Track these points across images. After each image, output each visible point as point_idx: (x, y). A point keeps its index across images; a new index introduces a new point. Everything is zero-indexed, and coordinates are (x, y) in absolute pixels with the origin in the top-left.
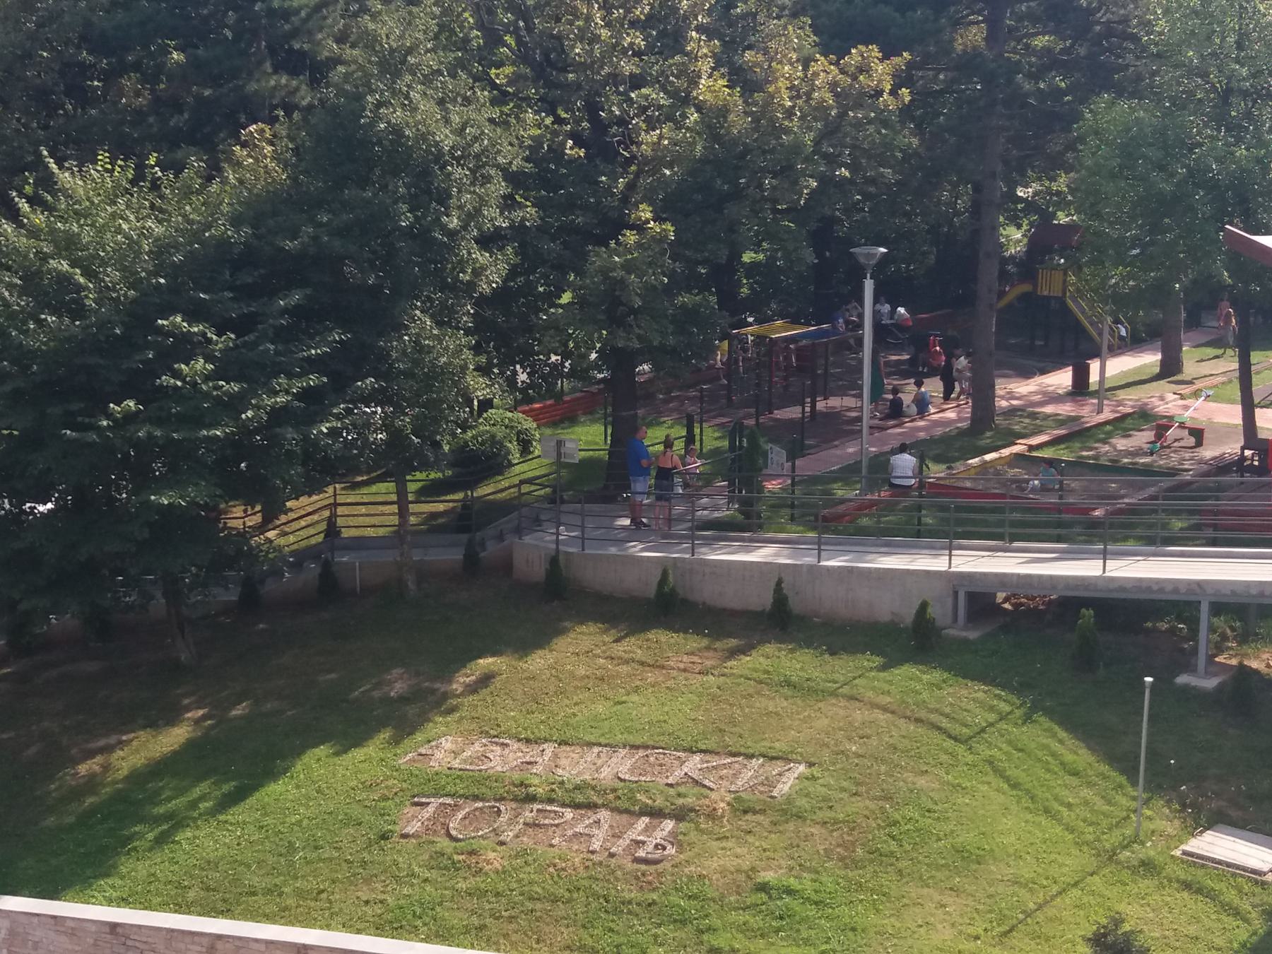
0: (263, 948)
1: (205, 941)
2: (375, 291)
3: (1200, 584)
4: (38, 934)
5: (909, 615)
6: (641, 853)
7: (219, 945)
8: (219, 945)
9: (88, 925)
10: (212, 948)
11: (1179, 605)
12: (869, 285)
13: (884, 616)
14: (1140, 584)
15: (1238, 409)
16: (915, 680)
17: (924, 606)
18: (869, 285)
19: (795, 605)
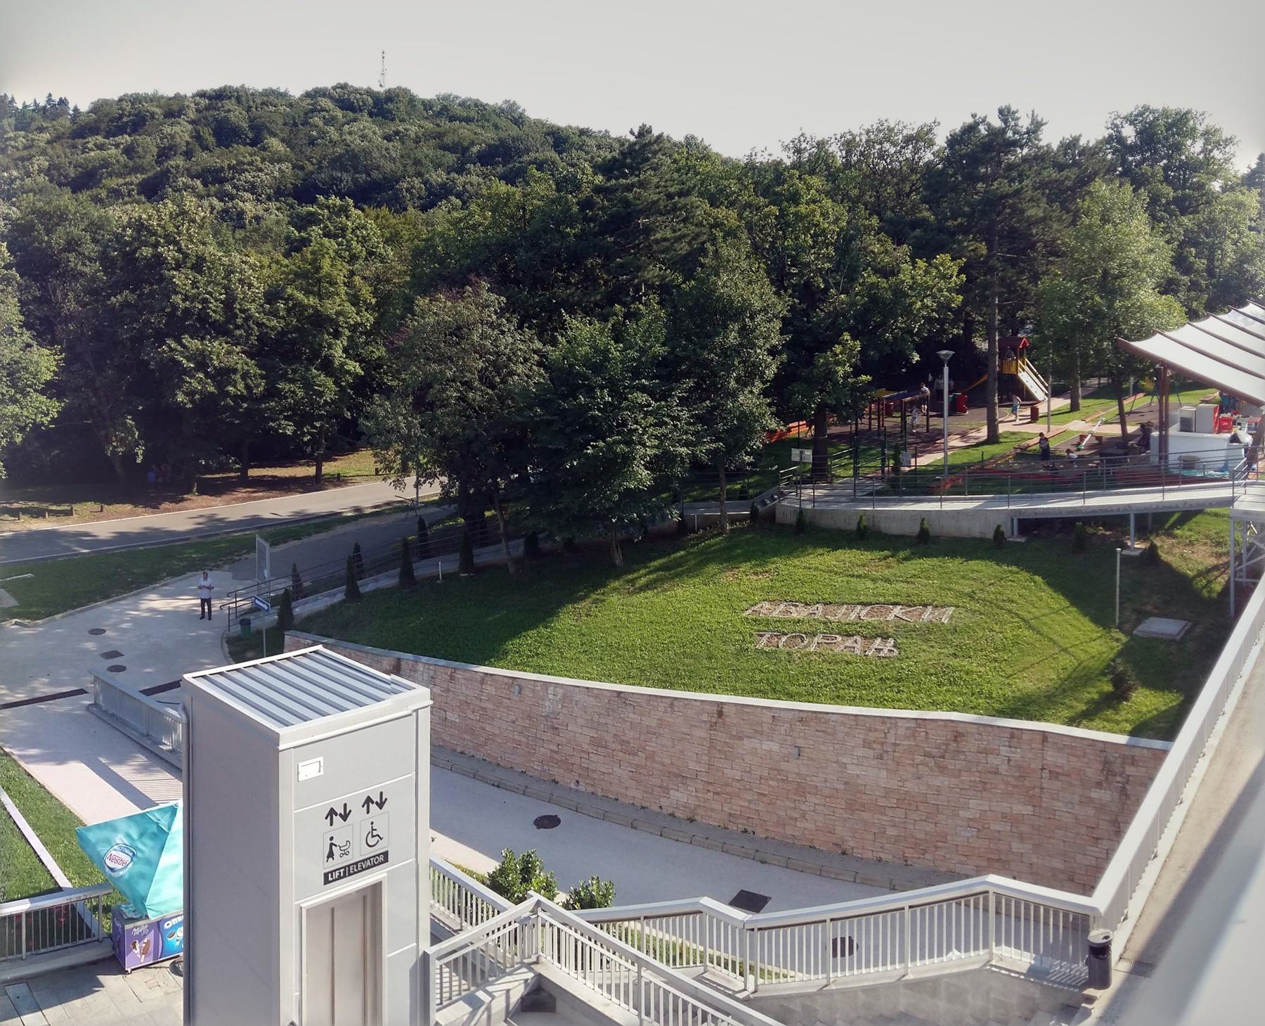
0: (913, 725)
1: (668, 701)
2: (614, 565)
3: (1129, 505)
4: (577, 697)
5: (990, 535)
6: (882, 654)
7: (676, 703)
8: (676, 703)
9: (782, 713)
10: (672, 705)
11: (1115, 520)
12: (946, 369)
13: (977, 535)
14: (1102, 508)
15: (1119, 426)
16: (983, 569)
17: (999, 527)
18: (946, 369)
19: (932, 532)
